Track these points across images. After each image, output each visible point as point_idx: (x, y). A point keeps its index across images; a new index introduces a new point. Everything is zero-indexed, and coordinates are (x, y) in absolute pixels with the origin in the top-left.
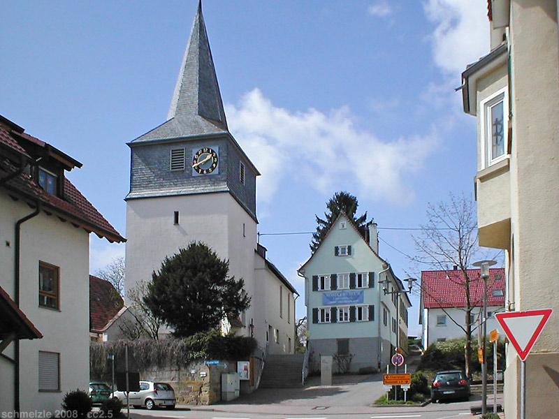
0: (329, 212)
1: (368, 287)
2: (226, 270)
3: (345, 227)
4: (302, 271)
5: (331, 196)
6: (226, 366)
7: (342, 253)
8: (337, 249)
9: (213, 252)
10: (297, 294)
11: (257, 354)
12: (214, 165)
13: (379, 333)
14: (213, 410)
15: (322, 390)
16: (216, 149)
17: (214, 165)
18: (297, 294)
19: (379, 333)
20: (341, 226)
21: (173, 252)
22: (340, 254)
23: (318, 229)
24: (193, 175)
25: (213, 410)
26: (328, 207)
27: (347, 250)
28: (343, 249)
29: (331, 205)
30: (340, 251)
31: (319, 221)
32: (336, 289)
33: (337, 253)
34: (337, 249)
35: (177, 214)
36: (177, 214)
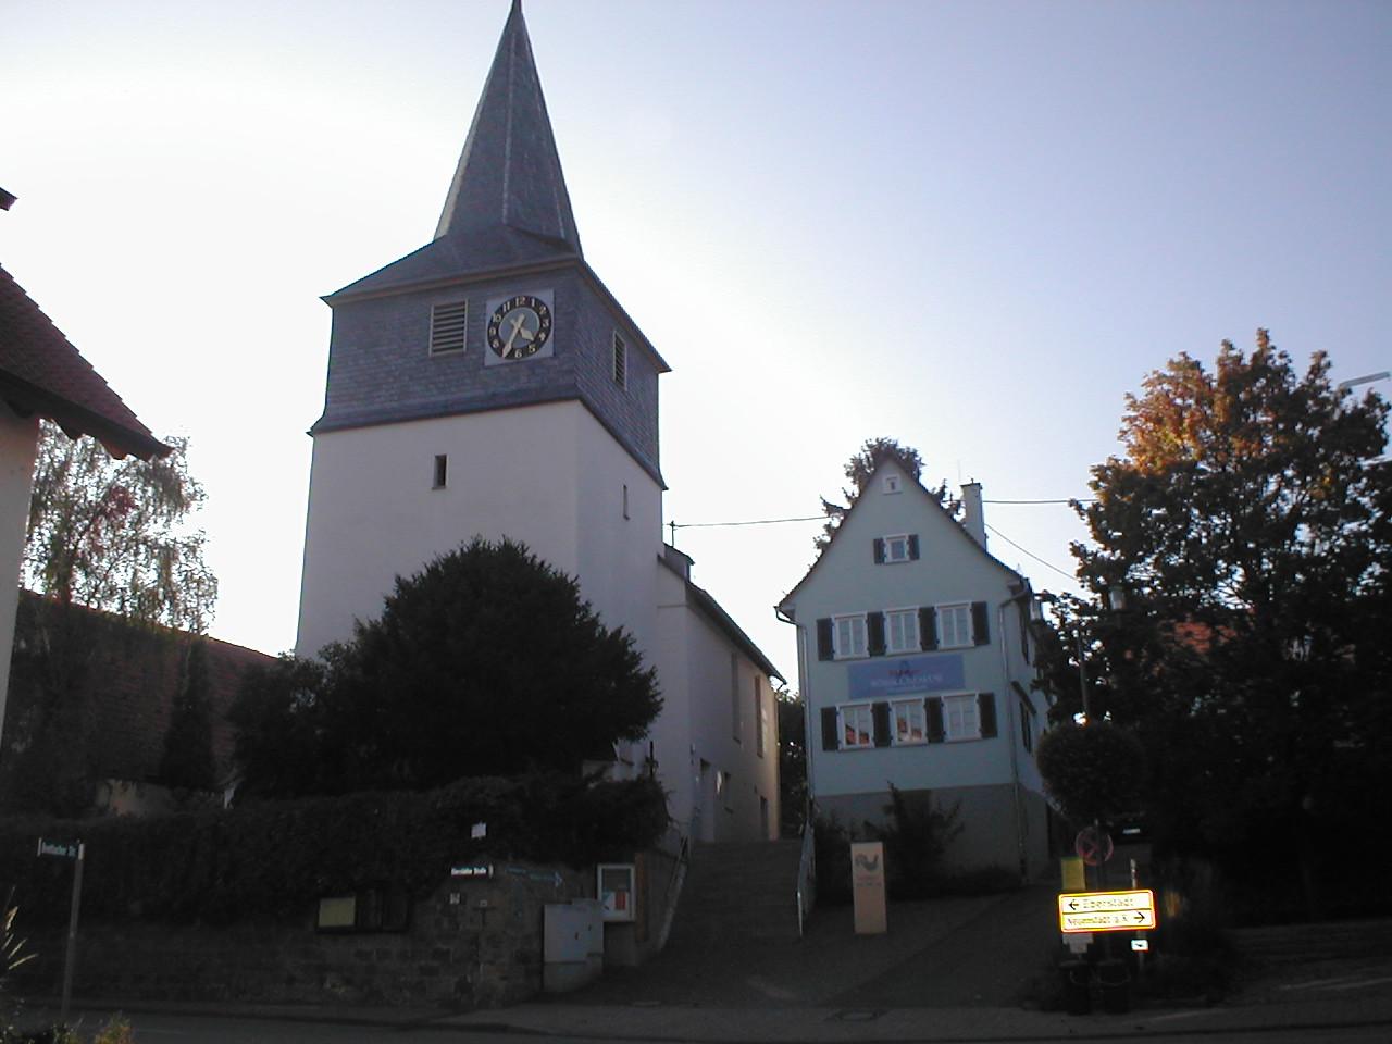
0: (854, 489)
1: (971, 643)
2: (637, 663)
3: (899, 487)
4: (788, 608)
5: (857, 449)
6: (558, 880)
7: (894, 556)
8: (879, 545)
9: (644, 667)
10: (780, 678)
11: (669, 843)
12: (542, 336)
13: (1016, 773)
14: (503, 1029)
15: (913, 625)
16: (547, 297)
17: (542, 336)
18: (780, 678)
19: (1016, 773)
20: (887, 488)
21: (415, 561)
22: (889, 558)
23: (828, 527)
24: (487, 363)
25: (503, 1029)
26: (848, 474)
27: (907, 548)
28: (897, 546)
29: (858, 471)
30: (888, 550)
31: (831, 509)
32: (883, 654)
33: (879, 557)
34: (879, 545)
35: (442, 462)
36: (442, 462)
